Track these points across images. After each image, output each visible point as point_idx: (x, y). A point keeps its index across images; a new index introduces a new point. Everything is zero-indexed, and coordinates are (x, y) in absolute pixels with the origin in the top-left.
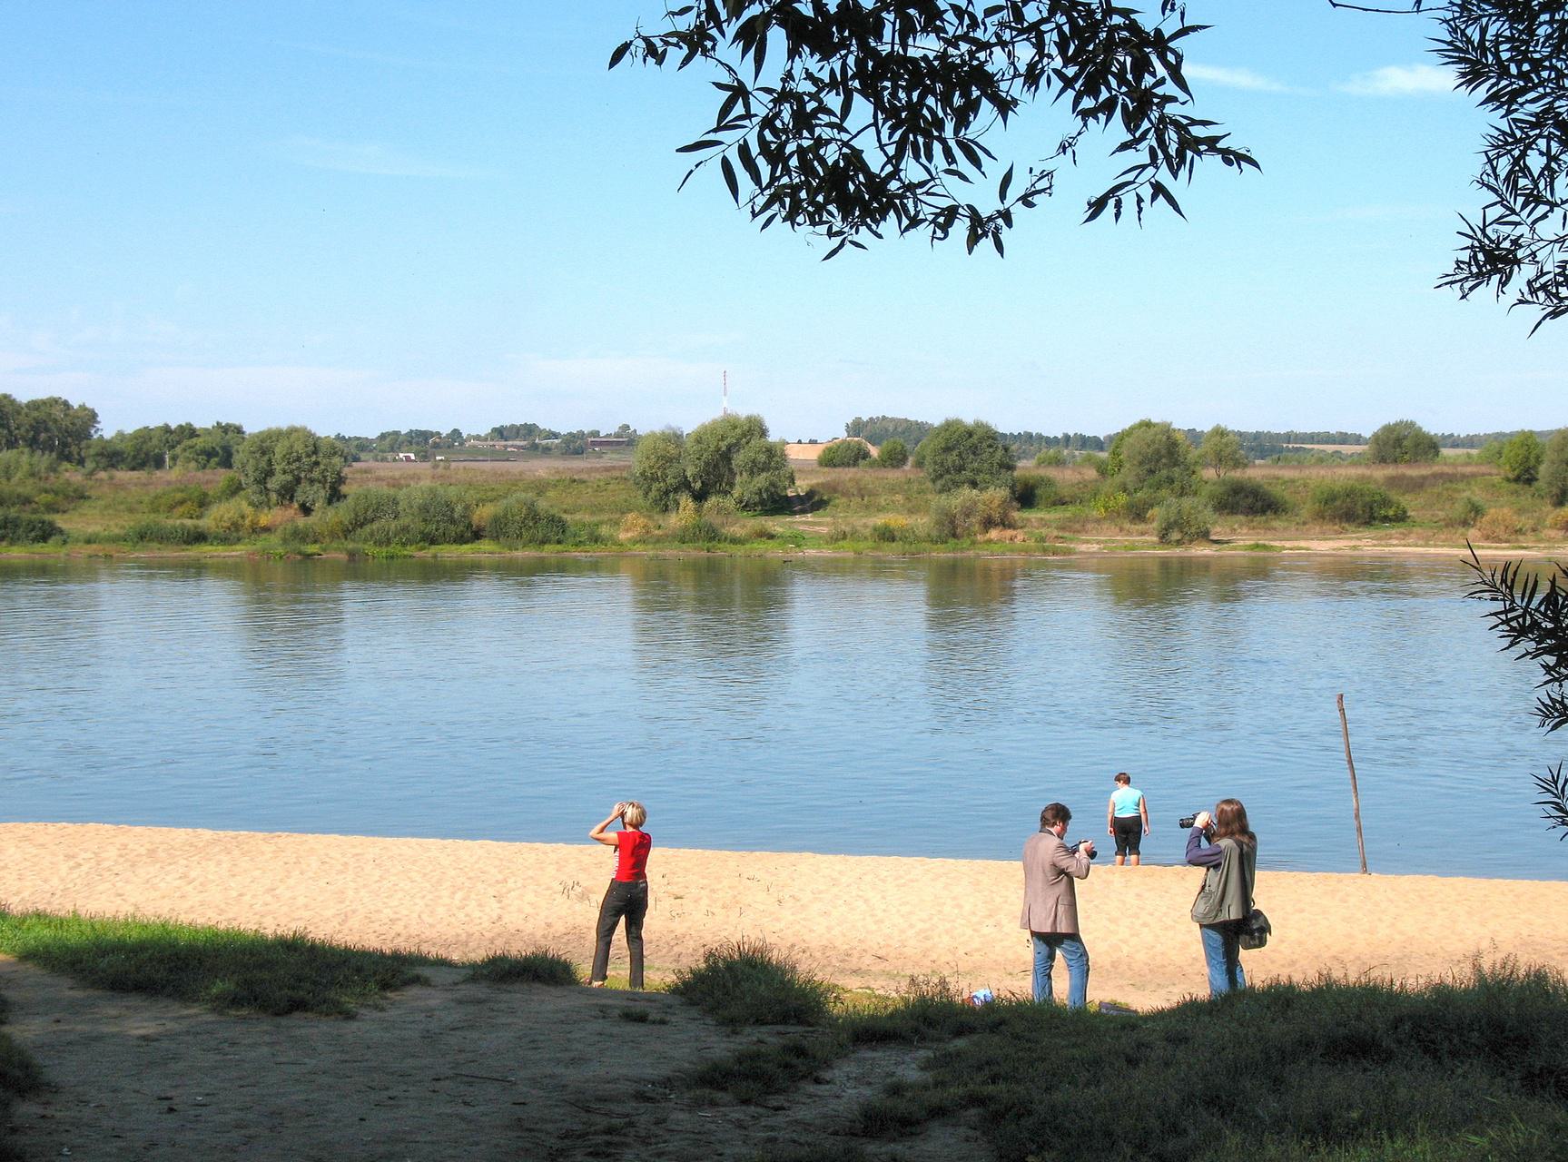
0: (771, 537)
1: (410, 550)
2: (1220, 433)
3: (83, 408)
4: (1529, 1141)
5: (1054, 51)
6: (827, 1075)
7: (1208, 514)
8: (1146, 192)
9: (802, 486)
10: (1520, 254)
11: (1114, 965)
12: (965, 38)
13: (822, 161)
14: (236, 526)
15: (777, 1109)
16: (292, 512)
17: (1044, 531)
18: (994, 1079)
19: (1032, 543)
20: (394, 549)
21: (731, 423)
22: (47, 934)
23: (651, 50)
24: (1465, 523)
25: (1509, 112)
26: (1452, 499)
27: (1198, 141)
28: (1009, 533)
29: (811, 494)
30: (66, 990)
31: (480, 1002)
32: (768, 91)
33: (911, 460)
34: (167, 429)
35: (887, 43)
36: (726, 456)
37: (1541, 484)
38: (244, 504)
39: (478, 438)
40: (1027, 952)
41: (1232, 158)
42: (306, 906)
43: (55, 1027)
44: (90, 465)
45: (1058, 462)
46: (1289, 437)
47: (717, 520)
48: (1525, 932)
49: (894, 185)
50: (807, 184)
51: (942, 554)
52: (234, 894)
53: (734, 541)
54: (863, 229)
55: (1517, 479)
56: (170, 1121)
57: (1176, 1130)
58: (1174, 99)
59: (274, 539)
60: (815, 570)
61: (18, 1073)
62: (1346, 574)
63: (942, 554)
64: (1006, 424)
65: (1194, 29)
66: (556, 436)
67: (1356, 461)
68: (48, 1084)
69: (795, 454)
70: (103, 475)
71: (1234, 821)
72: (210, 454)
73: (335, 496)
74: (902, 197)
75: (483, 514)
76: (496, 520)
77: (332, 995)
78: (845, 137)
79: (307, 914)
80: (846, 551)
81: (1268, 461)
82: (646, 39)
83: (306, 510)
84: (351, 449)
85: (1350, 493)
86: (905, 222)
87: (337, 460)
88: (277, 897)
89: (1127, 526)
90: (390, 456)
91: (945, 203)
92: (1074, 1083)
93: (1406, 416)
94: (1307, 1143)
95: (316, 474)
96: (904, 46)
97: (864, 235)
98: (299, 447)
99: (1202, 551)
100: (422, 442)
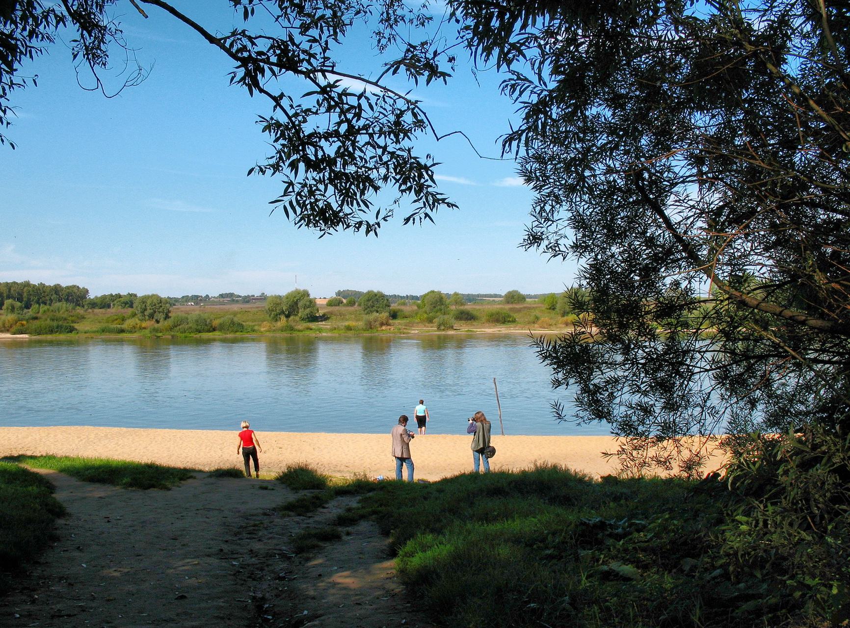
0: (311, 329)
1: (192, 335)
2: (456, 294)
3: (84, 288)
4: (550, 519)
5: (393, 171)
6: (327, 506)
7: (453, 321)
8: (423, 216)
9: (321, 312)
10: (543, 237)
11: (423, 467)
12: (363, 166)
13: (318, 206)
14: (134, 327)
15: (309, 517)
16: (153, 322)
17: (400, 327)
18: (381, 505)
19: (396, 330)
20: (187, 334)
21: (297, 292)
22: (68, 463)
23: (261, 170)
24: (534, 323)
25: (540, 192)
26: (529, 315)
27: (439, 200)
28: (389, 327)
29: (324, 315)
30: (74, 481)
31: (212, 484)
32: (299, 183)
33: (357, 304)
34: (111, 295)
35: (338, 167)
36: (296, 303)
37: (557, 310)
38: (137, 320)
39: (214, 297)
40: (394, 463)
41: (449, 205)
42: (157, 453)
43: (71, 494)
44: (86, 307)
45: (404, 304)
46: (478, 296)
47: (293, 324)
48: (553, 452)
49: (341, 214)
50: (313, 214)
51: (367, 334)
52: (133, 449)
53: (299, 331)
54: (331, 228)
55: (550, 309)
56: (109, 525)
57: (439, 521)
58: (431, 186)
59: (147, 331)
60: (326, 340)
61: (57, 510)
62: (496, 340)
63: (367, 334)
64: (388, 291)
65: (437, 164)
66: (240, 296)
67: (500, 303)
68: (68, 513)
69: (318, 302)
70: (90, 310)
71: (479, 418)
72: (126, 303)
73: (167, 317)
74: (344, 218)
75: (216, 323)
76: (220, 324)
77: (163, 482)
78: (325, 198)
79: (157, 455)
80: (336, 334)
81: (472, 303)
82: (259, 167)
83: (158, 322)
84: (172, 302)
85: (498, 313)
86: (345, 226)
87: (168, 305)
88: (148, 450)
89: (427, 324)
90: (185, 304)
91: (358, 220)
92: (406, 505)
93: (515, 289)
94: (480, 523)
95: (161, 310)
96: (344, 169)
97: (332, 230)
98: (155, 301)
99: (451, 332)
100: (196, 299)
